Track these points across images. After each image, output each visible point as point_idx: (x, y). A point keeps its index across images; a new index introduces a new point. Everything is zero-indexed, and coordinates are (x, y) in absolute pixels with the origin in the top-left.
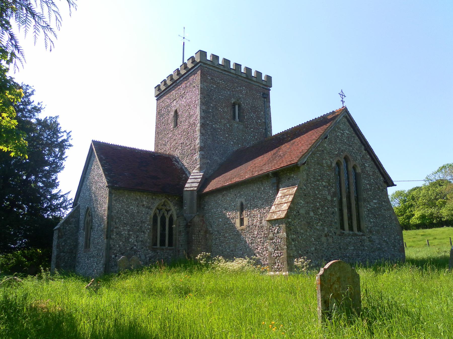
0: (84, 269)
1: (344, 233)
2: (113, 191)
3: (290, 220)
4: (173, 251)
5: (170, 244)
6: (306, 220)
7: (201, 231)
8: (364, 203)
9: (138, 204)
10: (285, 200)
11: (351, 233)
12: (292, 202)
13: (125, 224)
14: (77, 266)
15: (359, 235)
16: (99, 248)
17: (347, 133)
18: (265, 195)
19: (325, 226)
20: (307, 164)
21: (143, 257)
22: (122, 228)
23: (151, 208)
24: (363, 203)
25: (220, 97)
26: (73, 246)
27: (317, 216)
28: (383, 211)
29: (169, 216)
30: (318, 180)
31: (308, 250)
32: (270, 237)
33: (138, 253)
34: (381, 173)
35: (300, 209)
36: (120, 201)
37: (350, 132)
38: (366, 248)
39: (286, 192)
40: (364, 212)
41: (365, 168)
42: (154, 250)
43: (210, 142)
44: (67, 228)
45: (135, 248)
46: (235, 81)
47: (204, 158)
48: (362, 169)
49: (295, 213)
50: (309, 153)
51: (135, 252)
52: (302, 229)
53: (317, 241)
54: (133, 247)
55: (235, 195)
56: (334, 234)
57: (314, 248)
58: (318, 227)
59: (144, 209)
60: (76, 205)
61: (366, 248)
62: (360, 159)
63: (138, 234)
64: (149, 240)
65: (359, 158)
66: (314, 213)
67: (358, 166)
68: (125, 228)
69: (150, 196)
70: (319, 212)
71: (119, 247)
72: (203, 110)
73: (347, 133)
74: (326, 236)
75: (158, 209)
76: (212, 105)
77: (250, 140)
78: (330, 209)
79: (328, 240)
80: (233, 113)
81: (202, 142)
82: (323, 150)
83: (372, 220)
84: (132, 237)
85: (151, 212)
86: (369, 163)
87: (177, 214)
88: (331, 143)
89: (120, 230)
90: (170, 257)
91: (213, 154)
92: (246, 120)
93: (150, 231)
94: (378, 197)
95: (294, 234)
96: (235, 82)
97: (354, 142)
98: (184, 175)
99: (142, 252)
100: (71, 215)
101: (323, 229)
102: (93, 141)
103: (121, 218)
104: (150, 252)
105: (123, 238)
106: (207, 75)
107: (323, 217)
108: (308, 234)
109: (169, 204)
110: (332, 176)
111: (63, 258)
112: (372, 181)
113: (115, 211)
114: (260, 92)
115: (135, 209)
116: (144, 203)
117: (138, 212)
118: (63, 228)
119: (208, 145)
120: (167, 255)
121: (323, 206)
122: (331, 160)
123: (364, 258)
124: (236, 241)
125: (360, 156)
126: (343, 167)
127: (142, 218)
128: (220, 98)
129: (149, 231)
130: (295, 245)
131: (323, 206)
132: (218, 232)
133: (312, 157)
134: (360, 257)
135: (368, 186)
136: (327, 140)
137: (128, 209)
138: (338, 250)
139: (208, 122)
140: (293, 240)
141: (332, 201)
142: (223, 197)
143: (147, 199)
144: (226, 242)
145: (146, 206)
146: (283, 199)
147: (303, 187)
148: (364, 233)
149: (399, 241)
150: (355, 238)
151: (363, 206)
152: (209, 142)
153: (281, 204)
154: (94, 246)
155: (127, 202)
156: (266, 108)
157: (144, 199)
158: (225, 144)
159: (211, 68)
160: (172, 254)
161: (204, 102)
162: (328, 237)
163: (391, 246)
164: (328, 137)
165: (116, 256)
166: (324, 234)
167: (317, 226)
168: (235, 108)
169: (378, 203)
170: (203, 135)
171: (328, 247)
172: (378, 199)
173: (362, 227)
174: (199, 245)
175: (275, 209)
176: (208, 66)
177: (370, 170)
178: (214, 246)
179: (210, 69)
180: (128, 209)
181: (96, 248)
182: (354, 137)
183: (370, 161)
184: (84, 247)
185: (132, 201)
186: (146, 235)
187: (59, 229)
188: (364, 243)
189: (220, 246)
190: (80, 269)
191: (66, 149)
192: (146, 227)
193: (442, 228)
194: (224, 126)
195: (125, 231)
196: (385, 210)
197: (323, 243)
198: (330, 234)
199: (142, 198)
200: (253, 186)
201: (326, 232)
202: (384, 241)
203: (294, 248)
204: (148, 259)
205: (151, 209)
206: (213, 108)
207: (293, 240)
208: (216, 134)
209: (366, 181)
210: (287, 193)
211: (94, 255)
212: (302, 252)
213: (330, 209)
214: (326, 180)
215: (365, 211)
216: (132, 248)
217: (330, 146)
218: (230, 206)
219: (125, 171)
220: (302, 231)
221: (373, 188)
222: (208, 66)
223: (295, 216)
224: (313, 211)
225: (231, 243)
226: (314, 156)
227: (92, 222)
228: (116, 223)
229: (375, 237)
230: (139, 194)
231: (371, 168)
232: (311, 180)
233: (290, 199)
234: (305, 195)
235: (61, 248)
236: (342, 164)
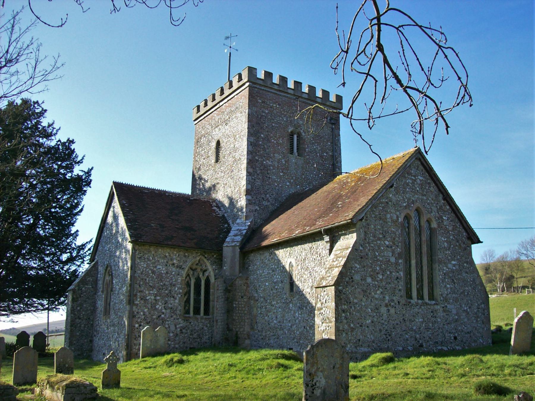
0: (103, 339)
2: (137, 247)
3: (340, 288)
4: (210, 321)
5: (207, 312)
6: (361, 287)
7: (244, 297)
8: (439, 266)
9: (167, 262)
11: (420, 301)
12: (345, 266)
13: (151, 286)
14: (95, 336)
15: (431, 305)
16: (120, 316)
17: (420, 180)
19: (385, 294)
20: (366, 220)
21: (173, 328)
22: (147, 292)
23: (182, 267)
24: (437, 266)
25: (274, 125)
26: (89, 312)
27: (376, 283)
28: (464, 274)
29: (206, 277)
30: (379, 239)
33: (167, 322)
34: (464, 228)
35: (354, 275)
36: (145, 259)
37: (424, 177)
38: (439, 320)
39: (339, 254)
40: (439, 277)
41: (442, 221)
42: (186, 320)
43: (260, 184)
44: (83, 289)
45: (163, 316)
46: (293, 104)
47: (251, 204)
48: (439, 224)
49: (347, 279)
50: (368, 207)
51: (163, 322)
52: (356, 298)
53: (375, 312)
54: (160, 316)
57: (370, 321)
58: (377, 296)
59: (174, 269)
60: (93, 261)
61: (439, 320)
63: (167, 299)
64: (180, 307)
66: (372, 278)
67: (433, 220)
68: (151, 292)
69: (182, 253)
70: (379, 278)
71: (144, 315)
72: (251, 142)
74: (386, 306)
75: (191, 268)
76: (262, 136)
77: (312, 179)
78: (393, 274)
79: (389, 311)
81: (249, 184)
82: (387, 202)
83: (448, 286)
84: (160, 304)
85: (183, 272)
86: (449, 215)
87: (215, 276)
89: (145, 295)
90: (206, 328)
91: (263, 198)
92: (307, 153)
93: (181, 296)
94: (459, 257)
95: (345, 304)
98: (226, 225)
99: (171, 322)
100: (88, 272)
101: (384, 297)
102: (114, 182)
103: (146, 280)
105: (148, 304)
106: (256, 97)
107: (384, 283)
108: (364, 304)
109: (205, 263)
110: (397, 233)
111: (79, 325)
112: (451, 237)
113: (139, 272)
115: (164, 269)
116: (175, 261)
117: (167, 273)
118: (79, 289)
119: (257, 187)
120: (202, 325)
121: (384, 271)
122: (398, 213)
123: (435, 332)
124: (284, 310)
125: (437, 207)
126: (414, 222)
127: (171, 280)
128: (273, 126)
129: (180, 296)
130: (345, 317)
131: (384, 271)
132: (264, 299)
133: (373, 211)
134: (430, 330)
135: (446, 244)
136: (393, 190)
137: (155, 269)
139: (257, 158)
140: (344, 311)
141: (397, 264)
143: (178, 256)
144: (273, 311)
145: (176, 265)
146: (335, 262)
149: (484, 310)
150: (425, 308)
151: (437, 269)
152: (258, 183)
154: (114, 313)
155: (153, 261)
156: (334, 137)
157: (175, 257)
158: (278, 185)
159: (262, 88)
160: (208, 325)
161: (252, 132)
163: (473, 317)
164: (395, 186)
165: (140, 326)
166: (384, 303)
167: (375, 294)
168: (293, 138)
169: (458, 265)
170: (250, 175)
172: (458, 259)
173: (435, 294)
174: (242, 314)
176: (258, 87)
177: (450, 224)
178: (259, 315)
179: (261, 89)
180: (155, 269)
181: (117, 315)
182: (429, 183)
183: (449, 213)
184: (103, 313)
185: (159, 259)
186: (177, 301)
187: (74, 291)
188: (437, 314)
189: (267, 315)
190: (99, 339)
191: (86, 171)
192: (176, 291)
194: (278, 163)
195: (151, 296)
196: (467, 273)
197: (382, 315)
198: (392, 304)
199: (171, 255)
201: (387, 301)
202: (464, 310)
203: (345, 321)
204: (179, 330)
205: (183, 269)
206: (263, 139)
207: (344, 311)
208: (268, 173)
209: (443, 239)
210: (340, 255)
211: (114, 324)
212: (354, 325)
213: (393, 274)
214: (389, 239)
215: (440, 275)
216: (159, 316)
217: (397, 196)
218: (278, 267)
219: (152, 222)
220: (355, 301)
221: (452, 246)
222: (258, 87)
223: (347, 283)
224: (371, 276)
225: (279, 313)
226: (375, 210)
227: (112, 283)
228: (140, 286)
230: (168, 250)
231: (451, 221)
232: (369, 239)
233: (342, 263)
234: (362, 258)
235: (76, 313)
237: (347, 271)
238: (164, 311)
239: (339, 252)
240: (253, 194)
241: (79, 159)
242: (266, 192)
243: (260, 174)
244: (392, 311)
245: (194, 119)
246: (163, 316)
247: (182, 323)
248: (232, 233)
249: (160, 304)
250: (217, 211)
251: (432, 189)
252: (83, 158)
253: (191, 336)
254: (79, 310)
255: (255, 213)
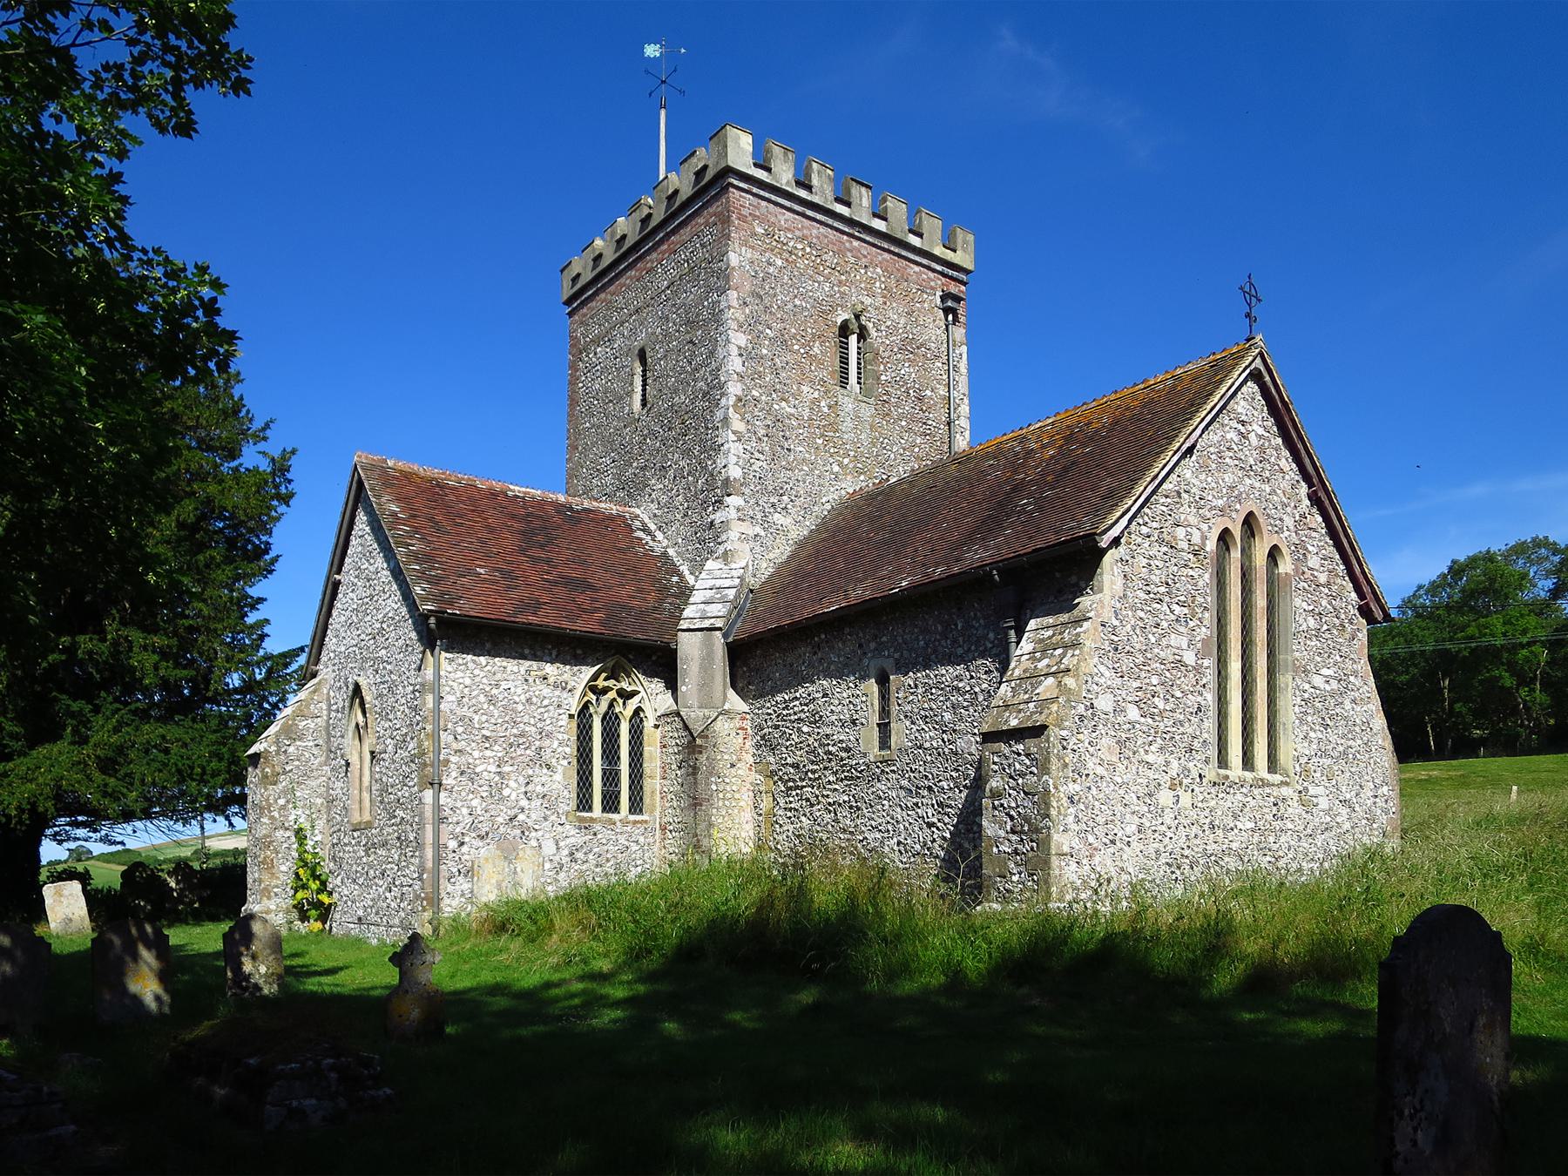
1: (1227, 777)
5: (636, 805)
10: (1048, 666)
11: (1248, 775)
18: (970, 649)
21: (549, 848)
23: (569, 687)
31: (1115, 831)
32: (991, 790)
33: (533, 834)
39: (1050, 638)
42: (585, 826)
47: (743, 520)
49: (1081, 709)
51: (523, 832)
55: (861, 646)
56: (1198, 780)
58: (1150, 758)
59: (546, 691)
62: (1292, 528)
65: (1289, 522)
68: (488, 753)
73: (1257, 435)
80: (841, 362)
84: (512, 784)
88: (1204, 468)
93: (569, 763)
96: (849, 250)
97: (1276, 467)
98: (675, 579)
101: (1167, 763)
104: (573, 832)
106: (750, 218)
111: (285, 845)
113: (451, 698)
114: (932, 288)
115: (519, 691)
118: (278, 752)
119: (758, 475)
122: (1204, 527)
129: (565, 763)
137: (495, 691)
138: (1207, 833)
139: (755, 393)
142: (815, 653)
147: (1110, 618)
148: (1288, 776)
153: (1034, 680)
162: (1179, 789)
171: (1177, 821)
175: (1009, 694)
180: (495, 691)
186: (558, 777)
193: (1395, 759)
200: (927, 617)
203: (1074, 827)
204: (566, 852)
229: (1320, 790)
235: (276, 814)
236: (1236, 543)
237: (1080, 687)
238: (524, 803)
239: (1050, 633)
240: (747, 491)
241: (257, 425)
242: (782, 488)
243: (766, 439)
244: (1186, 800)
245: (565, 298)
246: (521, 817)
247: (574, 837)
248: (697, 597)
249: (512, 784)
250: (647, 543)
251: (1283, 463)
252: (267, 426)
253: (598, 870)
254: (283, 807)
255: (752, 544)
